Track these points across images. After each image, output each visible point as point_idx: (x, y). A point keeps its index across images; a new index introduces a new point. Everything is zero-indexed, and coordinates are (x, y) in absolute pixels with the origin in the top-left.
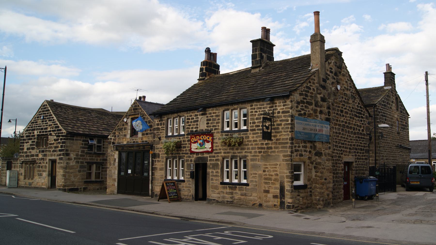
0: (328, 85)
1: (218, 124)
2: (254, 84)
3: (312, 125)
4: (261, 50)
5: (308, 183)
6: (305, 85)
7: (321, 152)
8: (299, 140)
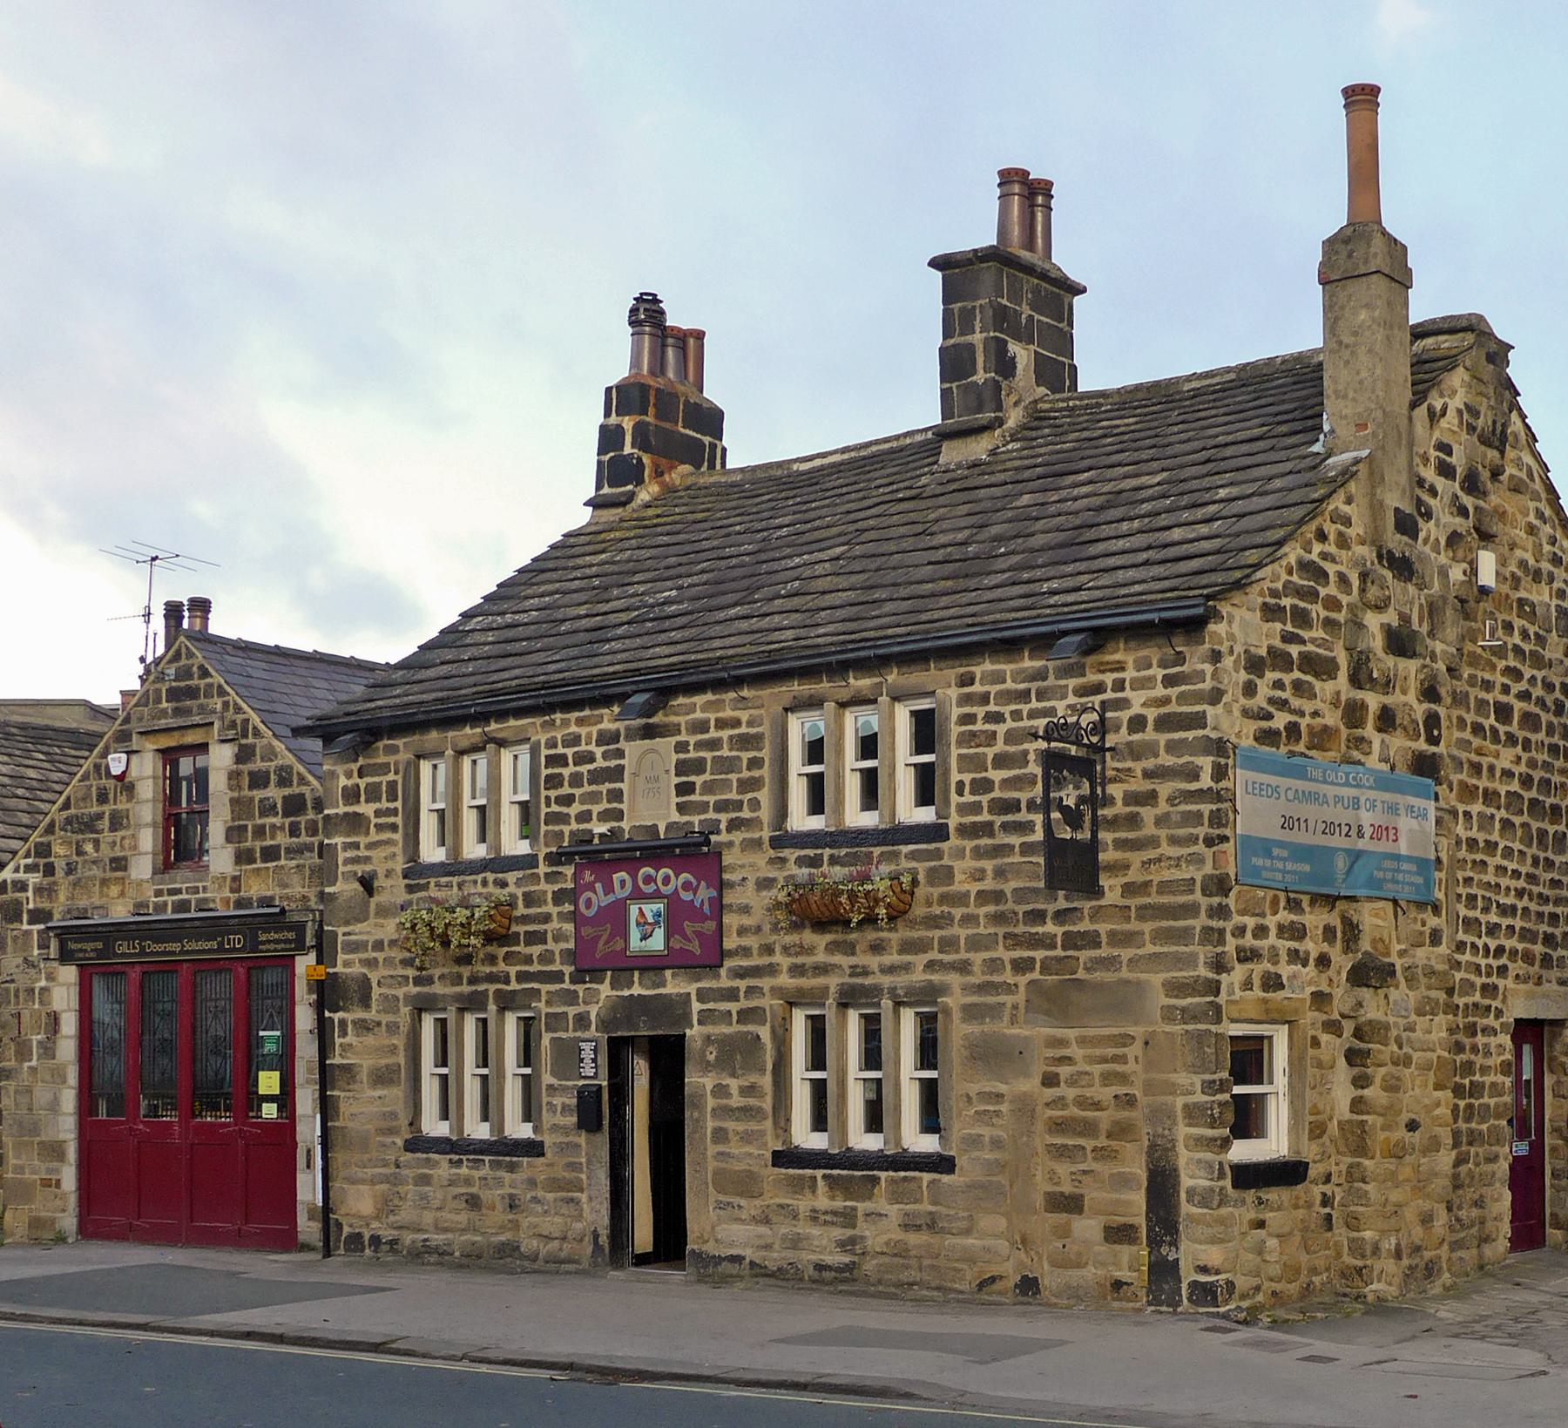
0: (1427, 549)
1: (750, 796)
2: (964, 543)
3: (1338, 799)
4: (1002, 318)
5: (1309, 1152)
6: (1292, 553)
7: (1387, 960)
8: (1261, 893)
